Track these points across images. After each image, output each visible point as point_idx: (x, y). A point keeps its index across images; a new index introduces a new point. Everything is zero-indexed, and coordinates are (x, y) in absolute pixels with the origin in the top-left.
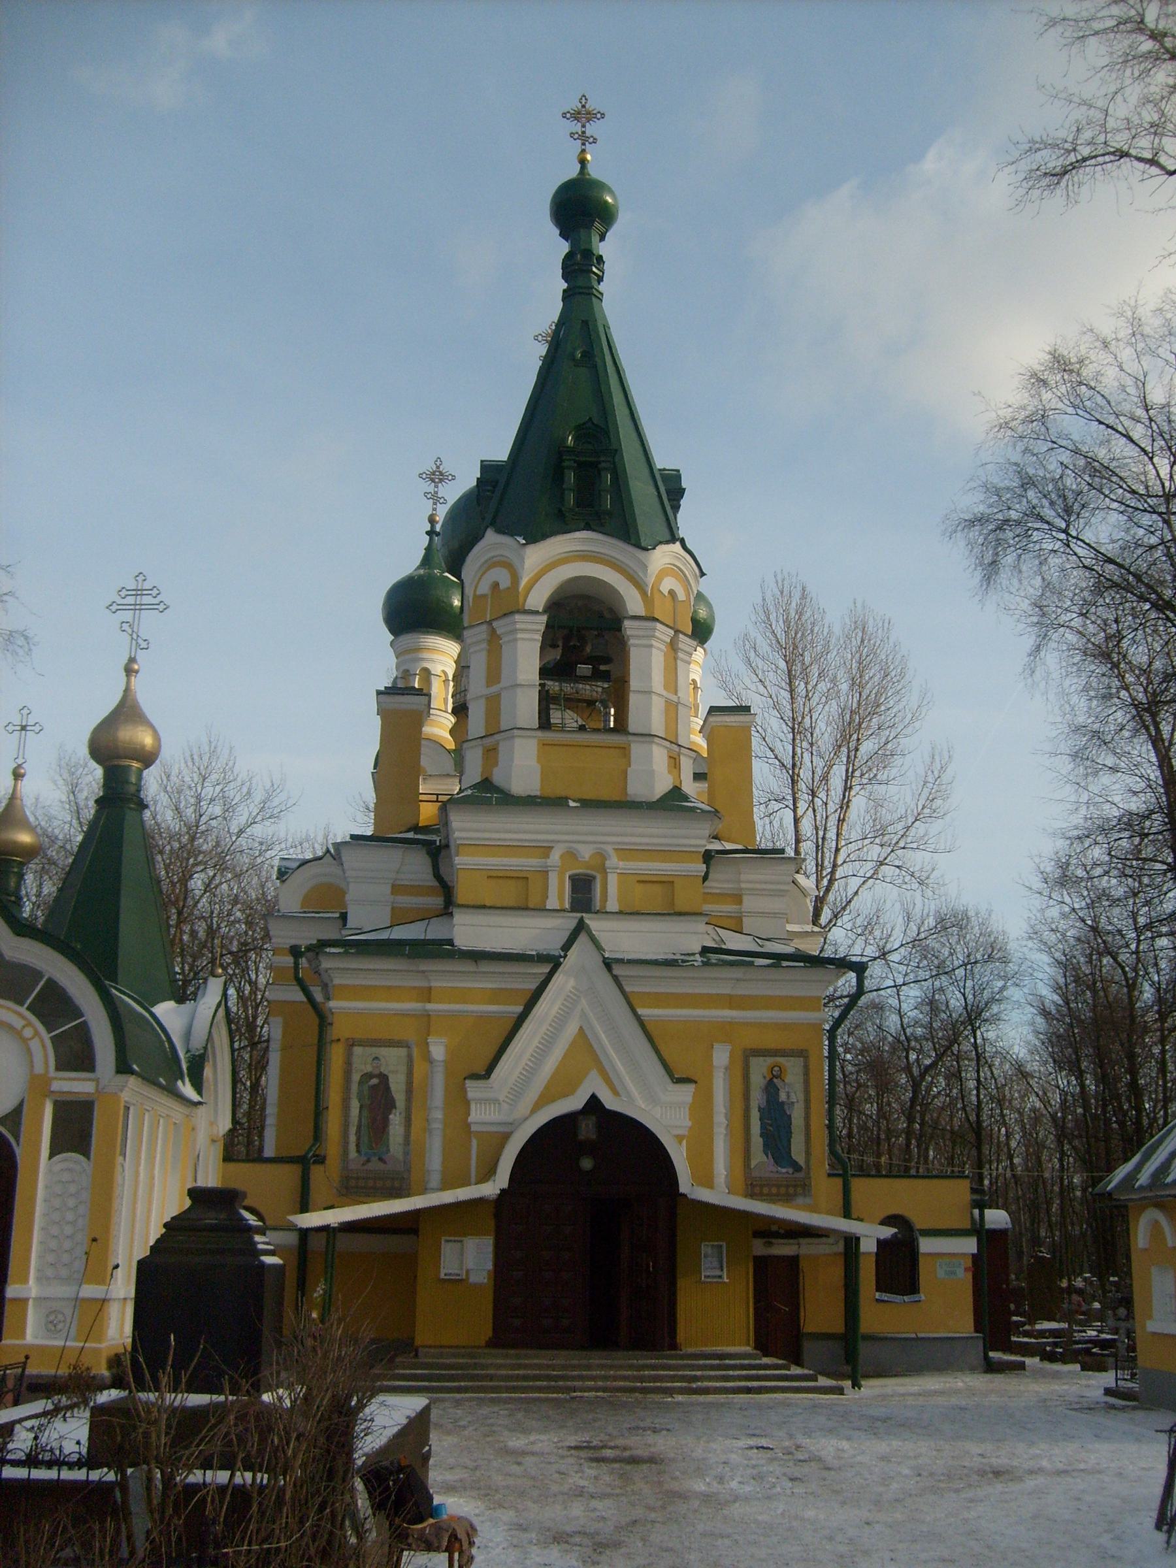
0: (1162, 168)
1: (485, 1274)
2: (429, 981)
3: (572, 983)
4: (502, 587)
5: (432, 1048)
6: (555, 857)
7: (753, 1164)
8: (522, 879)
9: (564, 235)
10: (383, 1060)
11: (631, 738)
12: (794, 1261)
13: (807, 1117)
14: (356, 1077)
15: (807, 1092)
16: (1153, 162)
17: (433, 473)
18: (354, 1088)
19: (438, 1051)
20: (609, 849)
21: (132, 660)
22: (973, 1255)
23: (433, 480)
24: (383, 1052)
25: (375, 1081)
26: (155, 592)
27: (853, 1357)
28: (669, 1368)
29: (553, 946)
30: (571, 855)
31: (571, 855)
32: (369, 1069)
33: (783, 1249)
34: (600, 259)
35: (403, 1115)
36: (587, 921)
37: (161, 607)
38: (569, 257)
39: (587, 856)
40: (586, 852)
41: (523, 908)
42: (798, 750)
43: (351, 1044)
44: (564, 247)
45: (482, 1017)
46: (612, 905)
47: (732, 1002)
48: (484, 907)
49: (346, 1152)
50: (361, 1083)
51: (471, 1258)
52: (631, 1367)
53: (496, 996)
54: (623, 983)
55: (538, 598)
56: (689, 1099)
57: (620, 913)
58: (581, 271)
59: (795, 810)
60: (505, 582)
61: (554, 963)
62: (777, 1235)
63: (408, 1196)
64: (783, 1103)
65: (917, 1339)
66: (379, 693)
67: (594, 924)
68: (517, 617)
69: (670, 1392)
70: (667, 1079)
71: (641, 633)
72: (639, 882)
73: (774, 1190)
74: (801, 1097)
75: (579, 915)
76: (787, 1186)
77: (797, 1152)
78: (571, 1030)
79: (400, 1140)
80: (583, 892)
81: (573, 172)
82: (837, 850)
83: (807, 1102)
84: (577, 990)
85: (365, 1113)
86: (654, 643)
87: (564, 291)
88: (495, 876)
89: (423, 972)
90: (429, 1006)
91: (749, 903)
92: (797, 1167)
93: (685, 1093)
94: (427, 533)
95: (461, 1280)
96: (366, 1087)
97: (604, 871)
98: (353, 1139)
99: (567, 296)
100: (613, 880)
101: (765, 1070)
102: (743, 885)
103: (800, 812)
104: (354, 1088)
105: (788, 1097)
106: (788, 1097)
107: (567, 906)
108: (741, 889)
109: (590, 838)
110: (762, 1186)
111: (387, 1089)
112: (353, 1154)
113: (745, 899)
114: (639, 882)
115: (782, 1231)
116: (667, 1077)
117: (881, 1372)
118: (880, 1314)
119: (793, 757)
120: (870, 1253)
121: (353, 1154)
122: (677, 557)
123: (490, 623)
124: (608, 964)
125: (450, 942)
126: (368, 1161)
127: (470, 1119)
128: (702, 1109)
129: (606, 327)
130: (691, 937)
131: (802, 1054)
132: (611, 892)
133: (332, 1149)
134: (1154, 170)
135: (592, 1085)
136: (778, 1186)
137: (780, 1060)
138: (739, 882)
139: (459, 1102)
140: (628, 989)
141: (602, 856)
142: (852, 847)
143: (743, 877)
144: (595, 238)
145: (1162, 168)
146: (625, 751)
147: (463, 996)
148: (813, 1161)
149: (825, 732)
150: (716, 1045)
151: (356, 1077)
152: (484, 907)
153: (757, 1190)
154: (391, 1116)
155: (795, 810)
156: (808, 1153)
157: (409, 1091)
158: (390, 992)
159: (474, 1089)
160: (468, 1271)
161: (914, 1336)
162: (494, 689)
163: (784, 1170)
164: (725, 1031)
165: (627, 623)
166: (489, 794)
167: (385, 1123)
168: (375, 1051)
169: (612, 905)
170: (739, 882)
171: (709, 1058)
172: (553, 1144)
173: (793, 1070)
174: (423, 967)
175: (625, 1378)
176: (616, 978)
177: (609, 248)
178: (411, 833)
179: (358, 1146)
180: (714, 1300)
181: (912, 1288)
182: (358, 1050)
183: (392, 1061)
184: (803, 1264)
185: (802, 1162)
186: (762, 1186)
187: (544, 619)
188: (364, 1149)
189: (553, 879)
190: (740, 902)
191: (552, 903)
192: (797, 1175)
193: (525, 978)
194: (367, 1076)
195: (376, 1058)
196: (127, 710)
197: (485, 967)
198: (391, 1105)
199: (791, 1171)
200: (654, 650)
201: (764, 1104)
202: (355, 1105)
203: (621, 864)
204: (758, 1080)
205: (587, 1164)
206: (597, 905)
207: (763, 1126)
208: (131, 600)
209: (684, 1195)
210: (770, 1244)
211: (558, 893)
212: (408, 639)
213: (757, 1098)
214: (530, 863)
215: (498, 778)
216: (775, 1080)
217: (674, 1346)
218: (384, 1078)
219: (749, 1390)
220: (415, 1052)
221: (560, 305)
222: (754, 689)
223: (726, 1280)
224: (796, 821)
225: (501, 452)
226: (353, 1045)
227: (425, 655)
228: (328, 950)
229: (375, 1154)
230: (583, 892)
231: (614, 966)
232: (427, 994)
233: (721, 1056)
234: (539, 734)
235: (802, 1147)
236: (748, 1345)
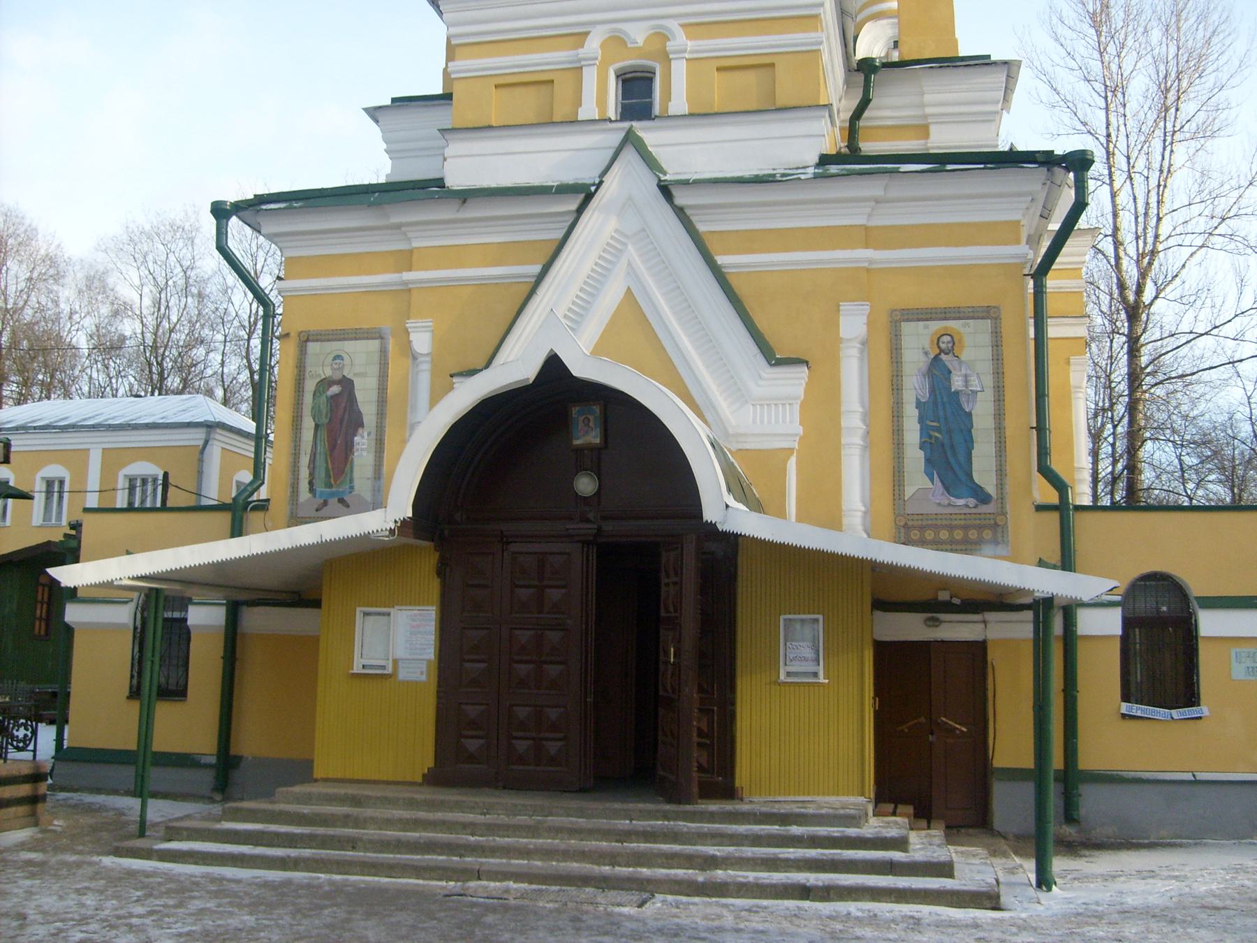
1: (424, 666)
2: (409, 239)
3: (612, 224)
5: (413, 337)
6: (593, 45)
7: (909, 491)
10: (347, 360)
12: (978, 650)
13: (999, 415)
14: (310, 385)
15: (998, 374)
18: (308, 399)
19: (421, 341)
20: (673, 25)
24: (349, 346)
25: (335, 389)
27: (1065, 815)
28: (675, 837)
29: (587, 176)
30: (617, 41)
31: (617, 41)
32: (328, 372)
35: (373, 436)
36: (641, 134)
39: (640, 41)
40: (638, 35)
41: (547, 123)
42: (1113, 119)
43: (306, 339)
45: (482, 286)
46: (679, 103)
47: (868, 236)
48: (490, 127)
51: (401, 639)
52: (606, 834)
53: (503, 253)
54: (694, 219)
56: (800, 391)
57: (691, 115)
59: (1111, 185)
61: (586, 194)
62: (948, 607)
64: (957, 393)
65: (1196, 782)
69: (647, 888)
70: (760, 359)
72: (718, 69)
73: (958, 535)
74: (989, 381)
75: (626, 125)
76: (966, 528)
77: (983, 472)
78: (611, 297)
79: (369, 472)
80: (637, 93)
82: (1159, 219)
83: (999, 390)
84: (622, 234)
85: (323, 434)
88: (506, 85)
89: (398, 227)
90: (407, 276)
93: (794, 382)
95: (390, 676)
96: (324, 398)
97: (666, 59)
98: (304, 473)
100: (679, 71)
101: (926, 342)
102: (928, 110)
103: (1117, 185)
104: (308, 399)
107: (612, 114)
108: (925, 116)
110: (922, 528)
111: (352, 399)
112: (304, 494)
113: (933, 130)
114: (718, 69)
115: (956, 601)
116: (760, 358)
117: (1127, 840)
118: (1118, 735)
119: (1107, 128)
120: (1114, 636)
121: (304, 494)
124: (665, 190)
125: (440, 183)
128: (822, 408)
131: (989, 313)
132: (676, 91)
136: (951, 528)
137: (953, 324)
138: (923, 106)
140: (701, 228)
141: (662, 36)
142: (1180, 217)
143: (928, 98)
147: (455, 256)
148: (1009, 488)
149: (1140, 87)
150: (844, 306)
151: (310, 385)
152: (490, 127)
153: (915, 535)
154: (356, 439)
155: (1111, 185)
156: (1001, 472)
157: (382, 401)
158: (358, 263)
160: (395, 662)
161: (1189, 777)
163: (961, 502)
164: (859, 283)
167: (349, 447)
168: (335, 346)
169: (679, 103)
170: (922, 106)
171: (832, 323)
173: (974, 343)
174: (395, 220)
175: (583, 855)
176: (680, 212)
179: (311, 483)
180: (803, 707)
181: (1187, 695)
182: (312, 347)
183: (359, 360)
184: (993, 655)
185: (991, 489)
186: (922, 528)
188: (320, 488)
190: (926, 135)
191: (588, 110)
192: (984, 509)
194: (326, 383)
197: (475, 211)
201: (925, 396)
202: (308, 424)
203: (690, 45)
204: (915, 358)
205: (585, 485)
206: (657, 110)
207: (924, 430)
209: (712, 526)
210: (935, 623)
211: (599, 94)
213: (914, 387)
214: (558, 57)
216: (943, 356)
217: (729, 792)
218: (347, 384)
219: (805, 892)
220: (391, 345)
222: (1062, 64)
223: (822, 679)
224: (1114, 195)
226: (307, 340)
228: (264, 207)
229: (332, 495)
230: (637, 93)
231: (675, 192)
232: (406, 260)
233: (853, 323)
235: (992, 464)
236: (862, 794)
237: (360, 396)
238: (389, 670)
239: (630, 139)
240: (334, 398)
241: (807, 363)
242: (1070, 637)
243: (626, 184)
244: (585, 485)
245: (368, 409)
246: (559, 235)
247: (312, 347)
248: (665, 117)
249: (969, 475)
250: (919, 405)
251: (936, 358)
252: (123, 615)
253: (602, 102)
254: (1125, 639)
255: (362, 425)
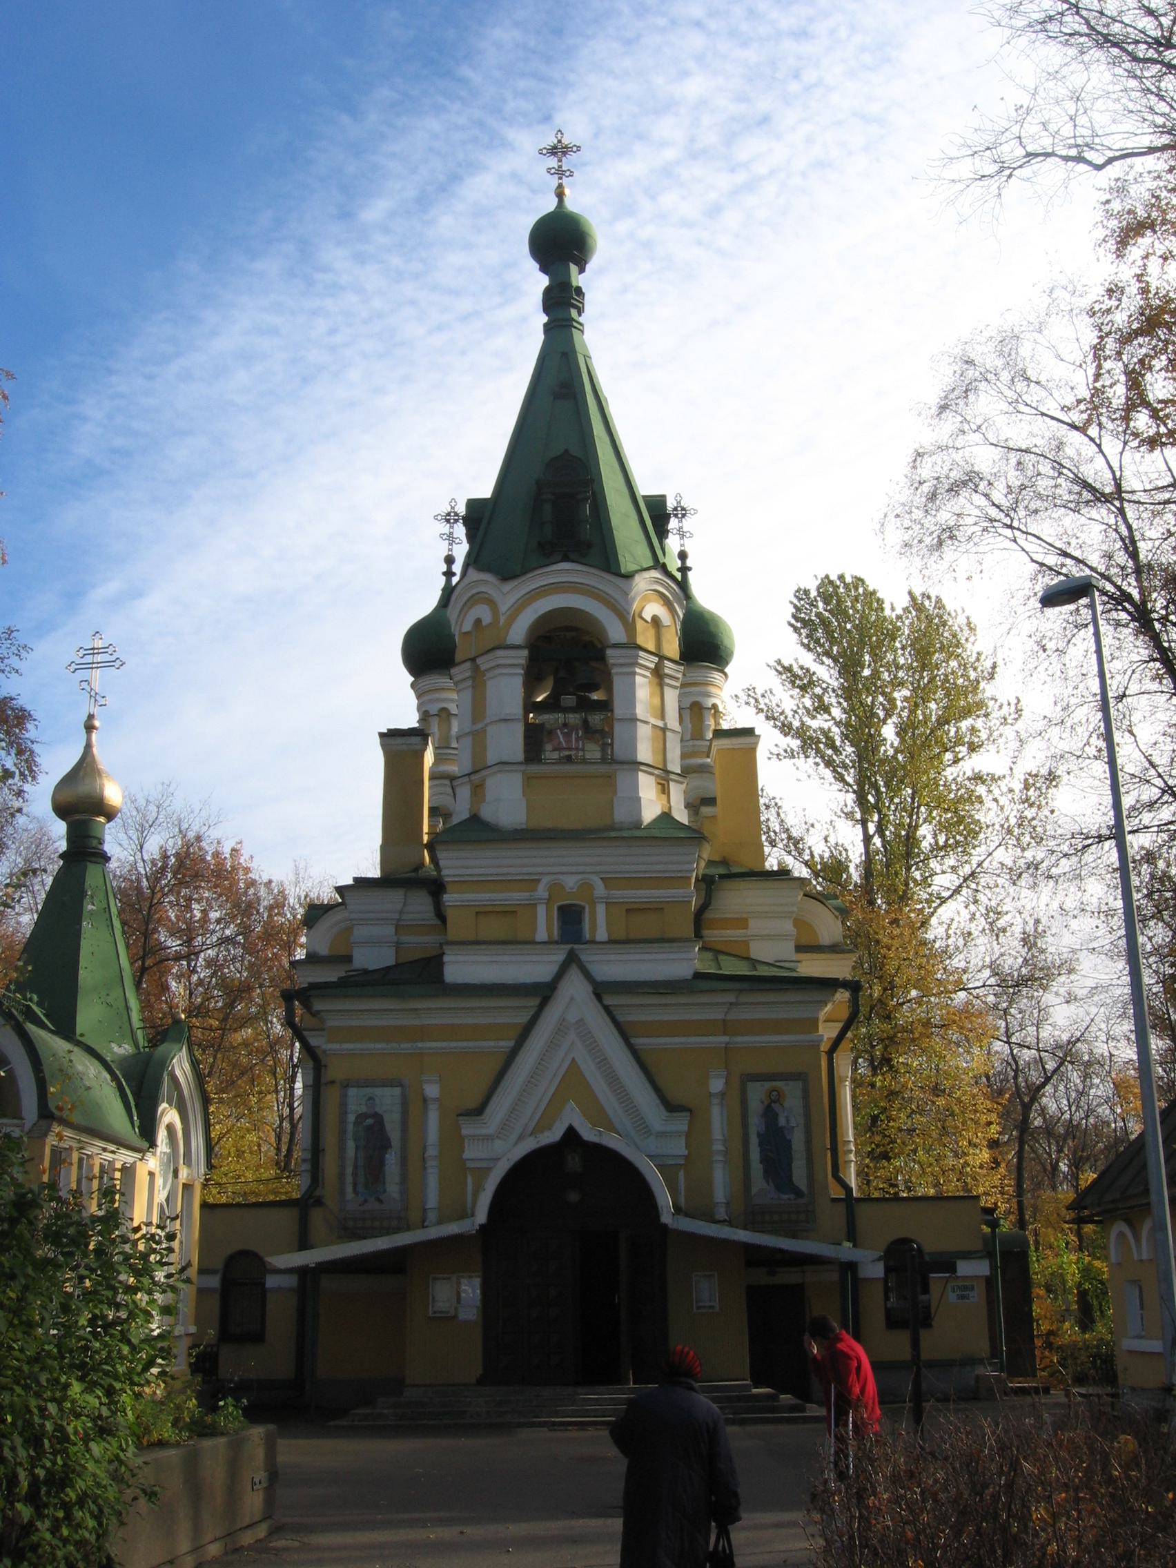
0: (1089, 163)
4: (484, 623)
6: (542, 891)
7: (754, 1190)
8: (508, 912)
9: (544, 269)
11: (615, 767)
16: (1079, 159)
17: (449, 514)
21: (91, 717)
22: (987, 1277)
23: (448, 521)
24: (378, 1091)
25: (370, 1121)
26: (111, 650)
30: (556, 888)
31: (556, 888)
32: (364, 1109)
33: (788, 1277)
34: (579, 291)
37: (118, 664)
38: (548, 292)
40: (570, 882)
44: (544, 281)
46: (602, 935)
49: (342, 1192)
50: (356, 1123)
51: (463, 1295)
55: (518, 632)
57: (611, 942)
58: (562, 304)
60: (487, 618)
63: (807, 1238)
64: (782, 1128)
66: (382, 735)
67: (588, 956)
68: (500, 653)
71: (621, 661)
74: (801, 1121)
75: (569, 947)
80: (571, 919)
81: (550, 205)
86: (638, 670)
87: (545, 325)
88: (482, 912)
91: (756, 926)
92: (798, 1193)
93: (680, 1124)
94: (444, 574)
99: (547, 328)
104: (350, 1127)
105: (788, 1121)
106: (788, 1121)
109: (574, 869)
113: (751, 923)
122: (657, 581)
123: (473, 660)
126: (366, 1201)
127: (465, 1156)
129: (587, 357)
130: (684, 963)
132: (599, 924)
133: (328, 1191)
134: (1082, 167)
135: (573, 1116)
139: (453, 1141)
144: (574, 268)
145: (1089, 163)
146: (610, 779)
151: (351, 1118)
159: (468, 1128)
162: (480, 726)
165: (609, 652)
166: (475, 832)
167: (382, 1163)
172: (535, 1178)
176: (607, 1010)
177: (593, 281)
178: (408, 872)
179: (355, 1185)
183: (387, 1100)
185: (804, 1188)
187: (525, 653)
189: (541, 911)
193: (514, 1014)
194: (361, 1117)
195: (370, 1098)
196: (85, 767)
198: (385, 1145)
199: (792, 1196)
200: (637, 677)
202: (351, 1145)
204: (756, 1106)
205: (574, 1197)
208: (89, 659)
211: (544, 925)
212: (696, 674)
213: (756, 1124)
214: (517, 896)
215: (487, 813)
218: (379, 1118)
221: (542, 337)
225: (485, 491)
227: (712, 690)
230: (571, 919)
234: (523, 767)
237: (388, 1127)
238: (452, 1313)
239: (572, 960)
240: (370, 1128)
241: (690, 1111)
242: (856, 1281)
243: (575, 989)
244: (574, 1197)
245: (394, 1135)
246: (523, 1018)
247: (352, 1091)
248: (593, 942)
249: (790, 1177)
250: (759, 1135)
251: (769, 1106)
252: (291, 1281)
253: (549, 929)
254: (886, 1280)
255: (390, 1146)
